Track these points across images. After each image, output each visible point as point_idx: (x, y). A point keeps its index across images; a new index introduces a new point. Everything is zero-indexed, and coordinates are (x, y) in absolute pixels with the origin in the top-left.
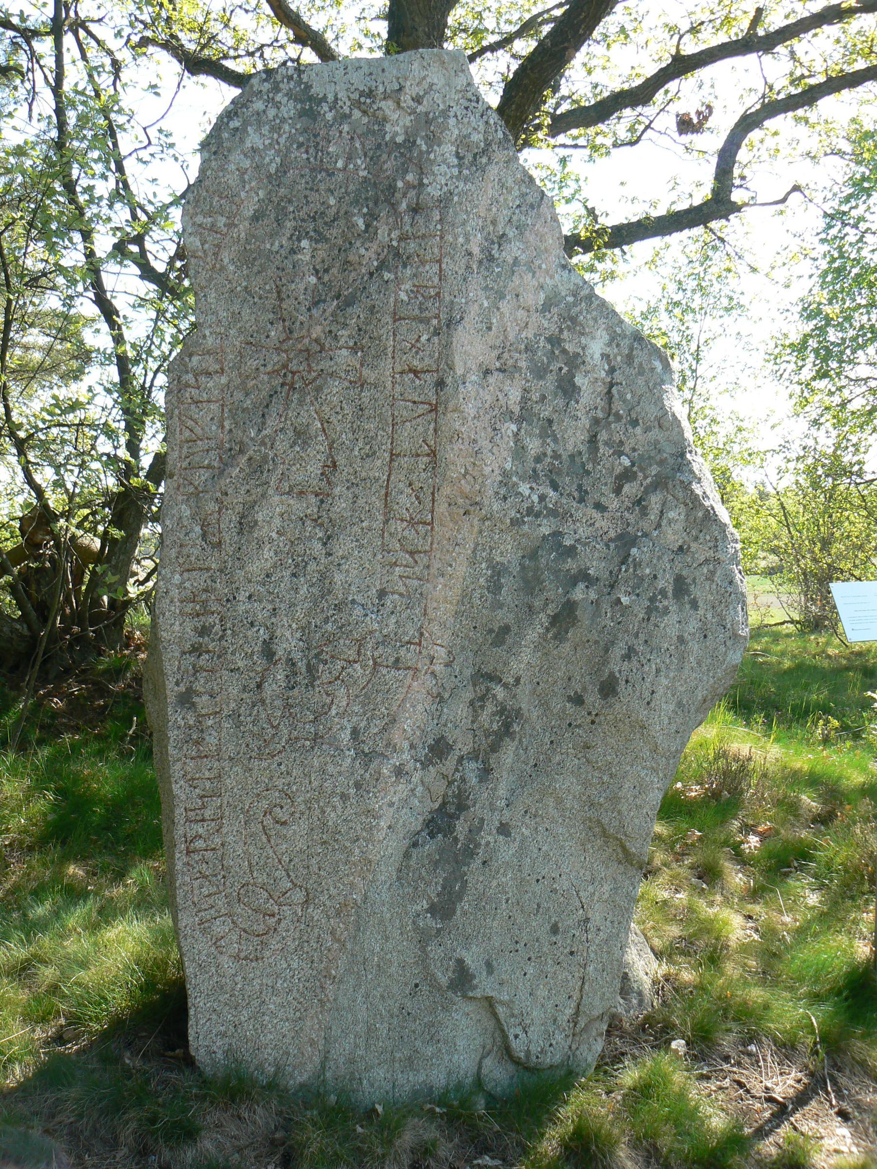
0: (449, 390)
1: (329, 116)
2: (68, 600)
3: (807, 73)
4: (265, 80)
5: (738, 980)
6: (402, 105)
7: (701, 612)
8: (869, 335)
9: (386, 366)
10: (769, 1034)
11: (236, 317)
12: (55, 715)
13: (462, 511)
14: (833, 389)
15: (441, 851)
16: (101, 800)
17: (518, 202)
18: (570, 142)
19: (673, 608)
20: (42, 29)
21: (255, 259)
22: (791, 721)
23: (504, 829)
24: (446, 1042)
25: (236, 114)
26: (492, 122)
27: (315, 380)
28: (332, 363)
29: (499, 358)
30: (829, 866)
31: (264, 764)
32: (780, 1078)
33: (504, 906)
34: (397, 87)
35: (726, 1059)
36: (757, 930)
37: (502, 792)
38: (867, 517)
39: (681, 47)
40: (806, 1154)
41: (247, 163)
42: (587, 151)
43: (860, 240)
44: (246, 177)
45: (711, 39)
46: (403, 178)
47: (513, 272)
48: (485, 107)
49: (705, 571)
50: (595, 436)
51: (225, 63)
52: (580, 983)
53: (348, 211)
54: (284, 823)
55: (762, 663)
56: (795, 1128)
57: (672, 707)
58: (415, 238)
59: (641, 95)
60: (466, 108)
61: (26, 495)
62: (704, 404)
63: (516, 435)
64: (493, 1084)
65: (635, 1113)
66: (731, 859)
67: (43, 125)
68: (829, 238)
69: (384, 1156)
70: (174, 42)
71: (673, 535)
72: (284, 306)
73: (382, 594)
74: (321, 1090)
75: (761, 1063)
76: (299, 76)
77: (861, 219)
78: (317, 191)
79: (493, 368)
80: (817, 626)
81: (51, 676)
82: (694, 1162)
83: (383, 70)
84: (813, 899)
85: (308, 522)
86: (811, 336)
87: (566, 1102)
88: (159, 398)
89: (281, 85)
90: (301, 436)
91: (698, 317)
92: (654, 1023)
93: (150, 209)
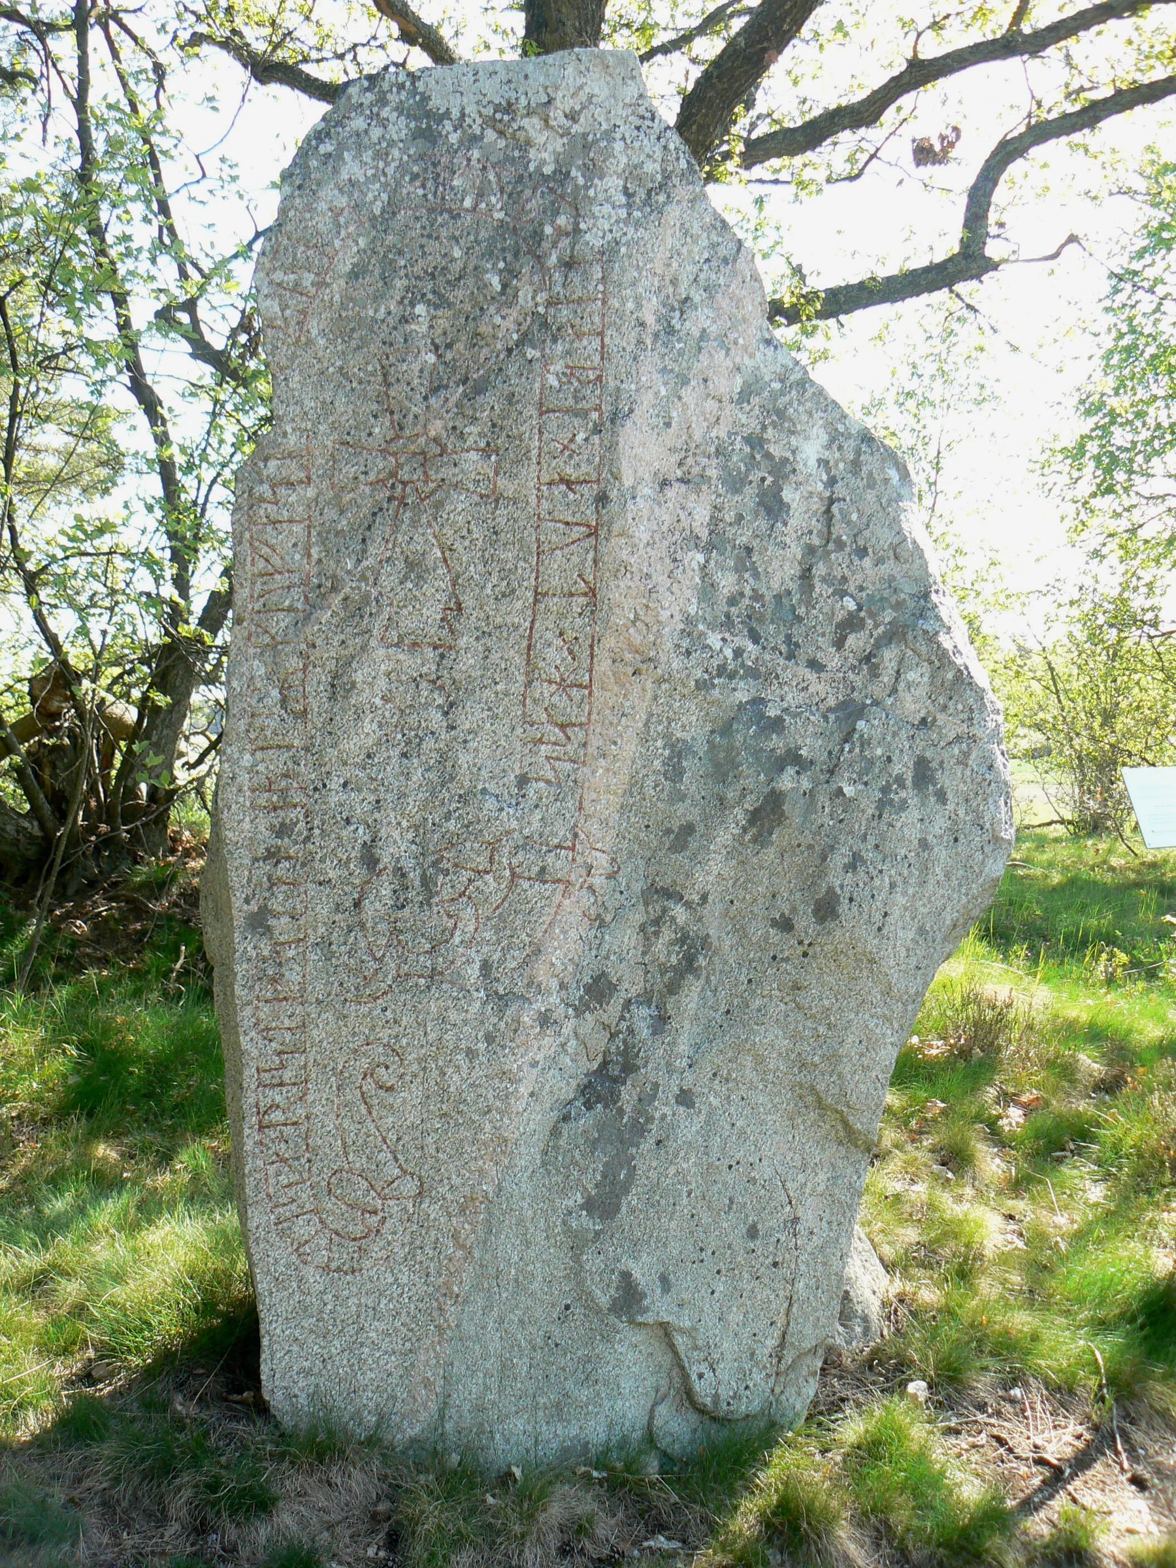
0: (614, 507)
1: (454, 138)
2: (93, 789)
3: (1087, 85)
4: (367, 89)
5: (997, 1301)
6: (552, 123)
7: (950, 806)
8: (1168, 437)
9: (529, 473)
10: (1038, 1374)
11: (328, 407)
12: (75, 943)
13: (630, 670)
14: (1119, 510)
15: (601, 1127)
16: (139, 1057)
17: (706, 255)
18: (769, 176)
19: (913, 801)
20: (61, 23)
21: (353, 330)
22: (1064, 955)
23: (685, 1098)
24: (606, 1383)
25: (328, 135)
26: (672, 146)
27: (433, 493)
28: (457, 471)
29: (680, 464)
30: (1116, 1148)
31: (364, 1009)
32: (1053, 1433)
33: (685, 1201)
34: (544, 99)
35: (982, 1407)
36: (1021, 1235)
37: (683, 1048)
38: (1164, 682)
39: (919, 48)
40: (1090, 1534)
41: (342, 201)
42: (792, 188)
43: (1157, 310)
44: (342, 220)
45: (958, 38)
46: (553, 222)
47: (700, 349)
48: (663, 126)
49: (956, 751)
50: (809, 570)
51: (305, 67)
52: (786, 1305)
53: (459, 269)
54: (390, 1089)
55: (1022, 877)
56: (1074, 1501)
57: (911, 935)
58: (568, 302)
59: (863, 114)
60: (638, 128)
61: (35, 648)
62: (945, 530)
63: (703, 568)
64: (669, 1439)
65: (860, 1479)
66: (986, 1139)
67: (61, 150)
68: (1115, 306)
69: (523, 1536)
70: (236, 39)
71: (913, 703)
72: (392, 394)
73: (523, 781)
74: (439, 1448)
75: (1028, 1413)
76: (413, 84)
77: (1158, 281)
78: (437, 238)
79: (672, 477)
80: (1096, 828)
81: (70, 892)
82: (939, 1545)
83: (526, 77)
84: (1097, 1193)
85: (424, 685)
86: (1091, 438)
87: (766, 1464)
88: (220, 519)
89: (389, 96)
90: (415, 568)
91: (938, 411)
92: (884, 1359)
93: (206, 264)
